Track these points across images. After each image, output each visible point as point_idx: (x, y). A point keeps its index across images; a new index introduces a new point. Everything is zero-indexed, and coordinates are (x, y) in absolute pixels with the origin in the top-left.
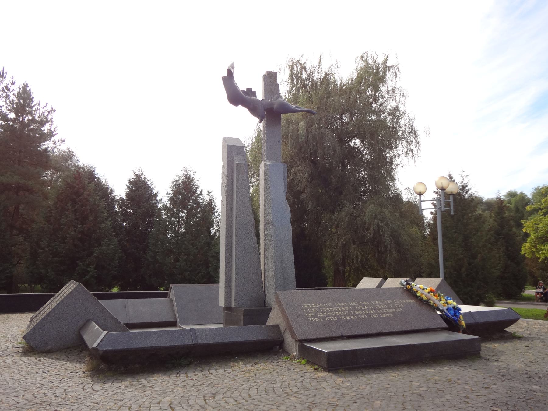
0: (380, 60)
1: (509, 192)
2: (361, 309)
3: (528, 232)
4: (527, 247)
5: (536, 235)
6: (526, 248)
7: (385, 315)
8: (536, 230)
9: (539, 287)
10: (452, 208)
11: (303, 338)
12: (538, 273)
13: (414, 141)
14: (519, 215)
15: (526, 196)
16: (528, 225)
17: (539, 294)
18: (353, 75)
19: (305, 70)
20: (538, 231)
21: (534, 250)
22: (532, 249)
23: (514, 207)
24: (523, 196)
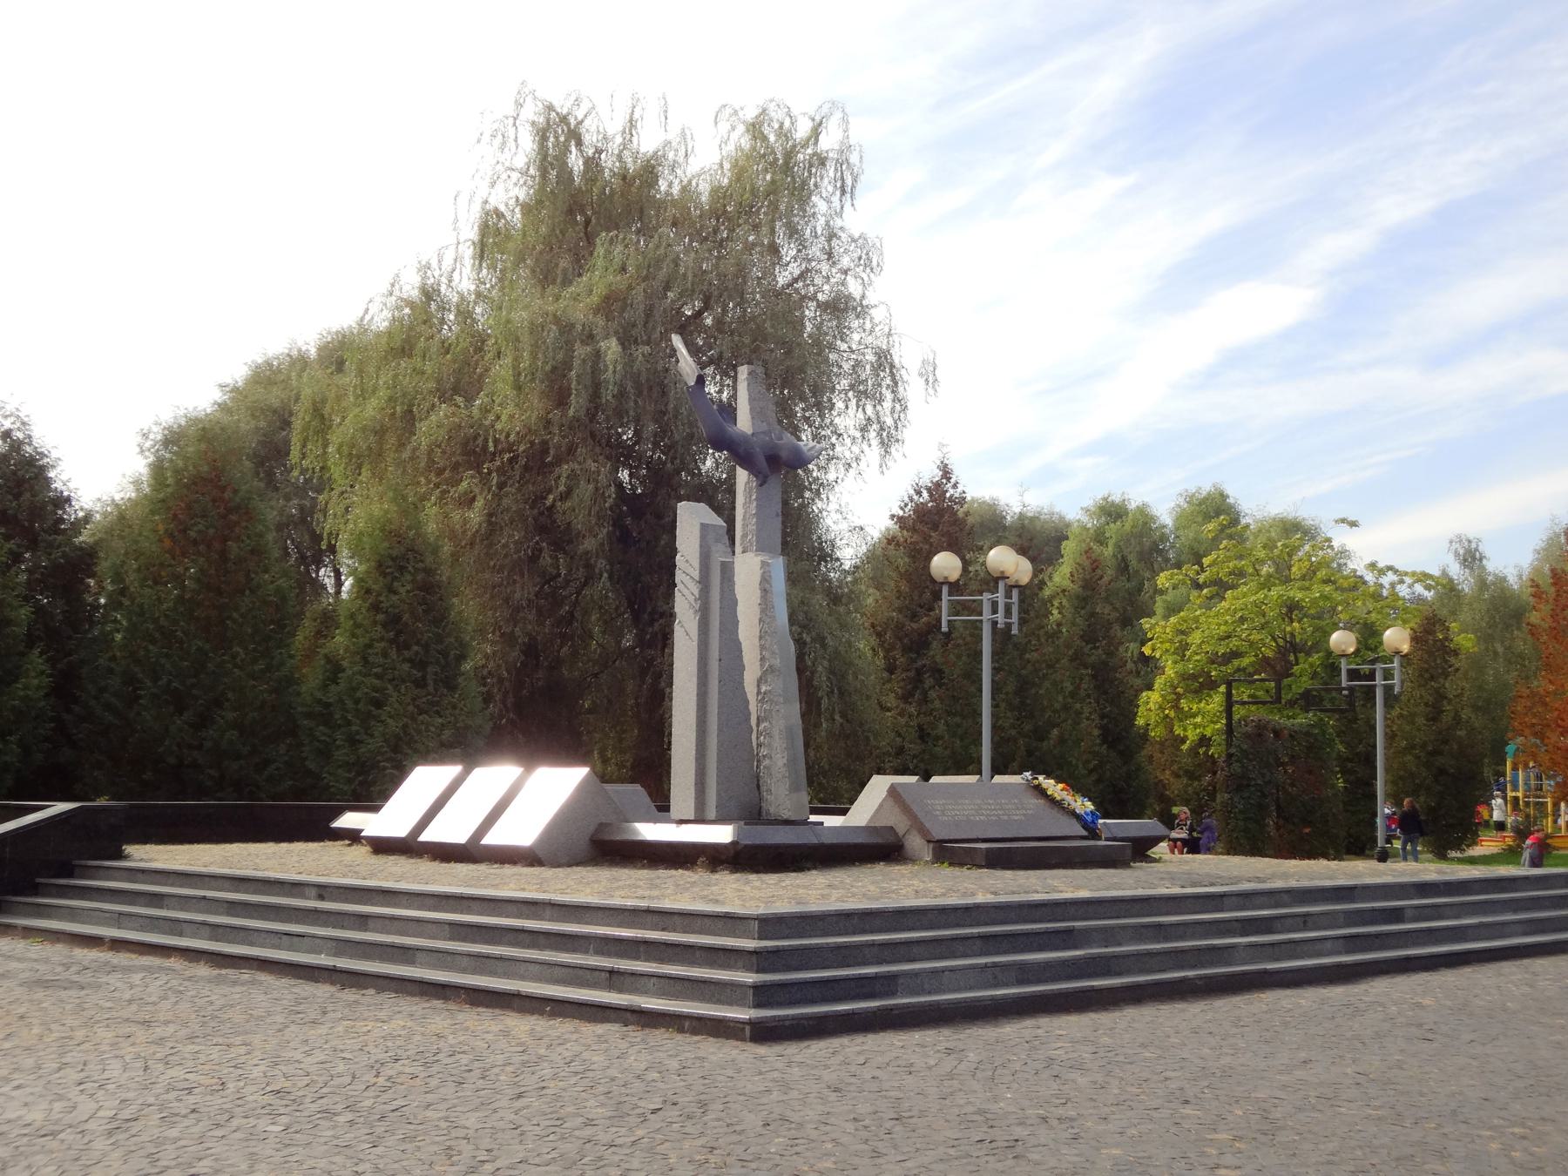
0: (802, 130)
1: (1105, 499)
2: (988, 809)
3: (1158, 656)
4: (1151, 705)
5: (1180, 667)
6: (1150, 704)
7: (1016, 818)
8: (1182, 650)
9: (1178, 825)
10: (1015, 619)
11: (941, 838)
12: (1176, 786)
13: (888, 395)
14: (1128, 585)
15: (1153, 519)
16: (1158, 630)
17: (1179, 843)
18: (742, 196)
19: (579, 143)
20: (1188, 653)
21: (1172, 714)
22: (1167, 712)
23: (1114, 556)
24: (1144, 518)
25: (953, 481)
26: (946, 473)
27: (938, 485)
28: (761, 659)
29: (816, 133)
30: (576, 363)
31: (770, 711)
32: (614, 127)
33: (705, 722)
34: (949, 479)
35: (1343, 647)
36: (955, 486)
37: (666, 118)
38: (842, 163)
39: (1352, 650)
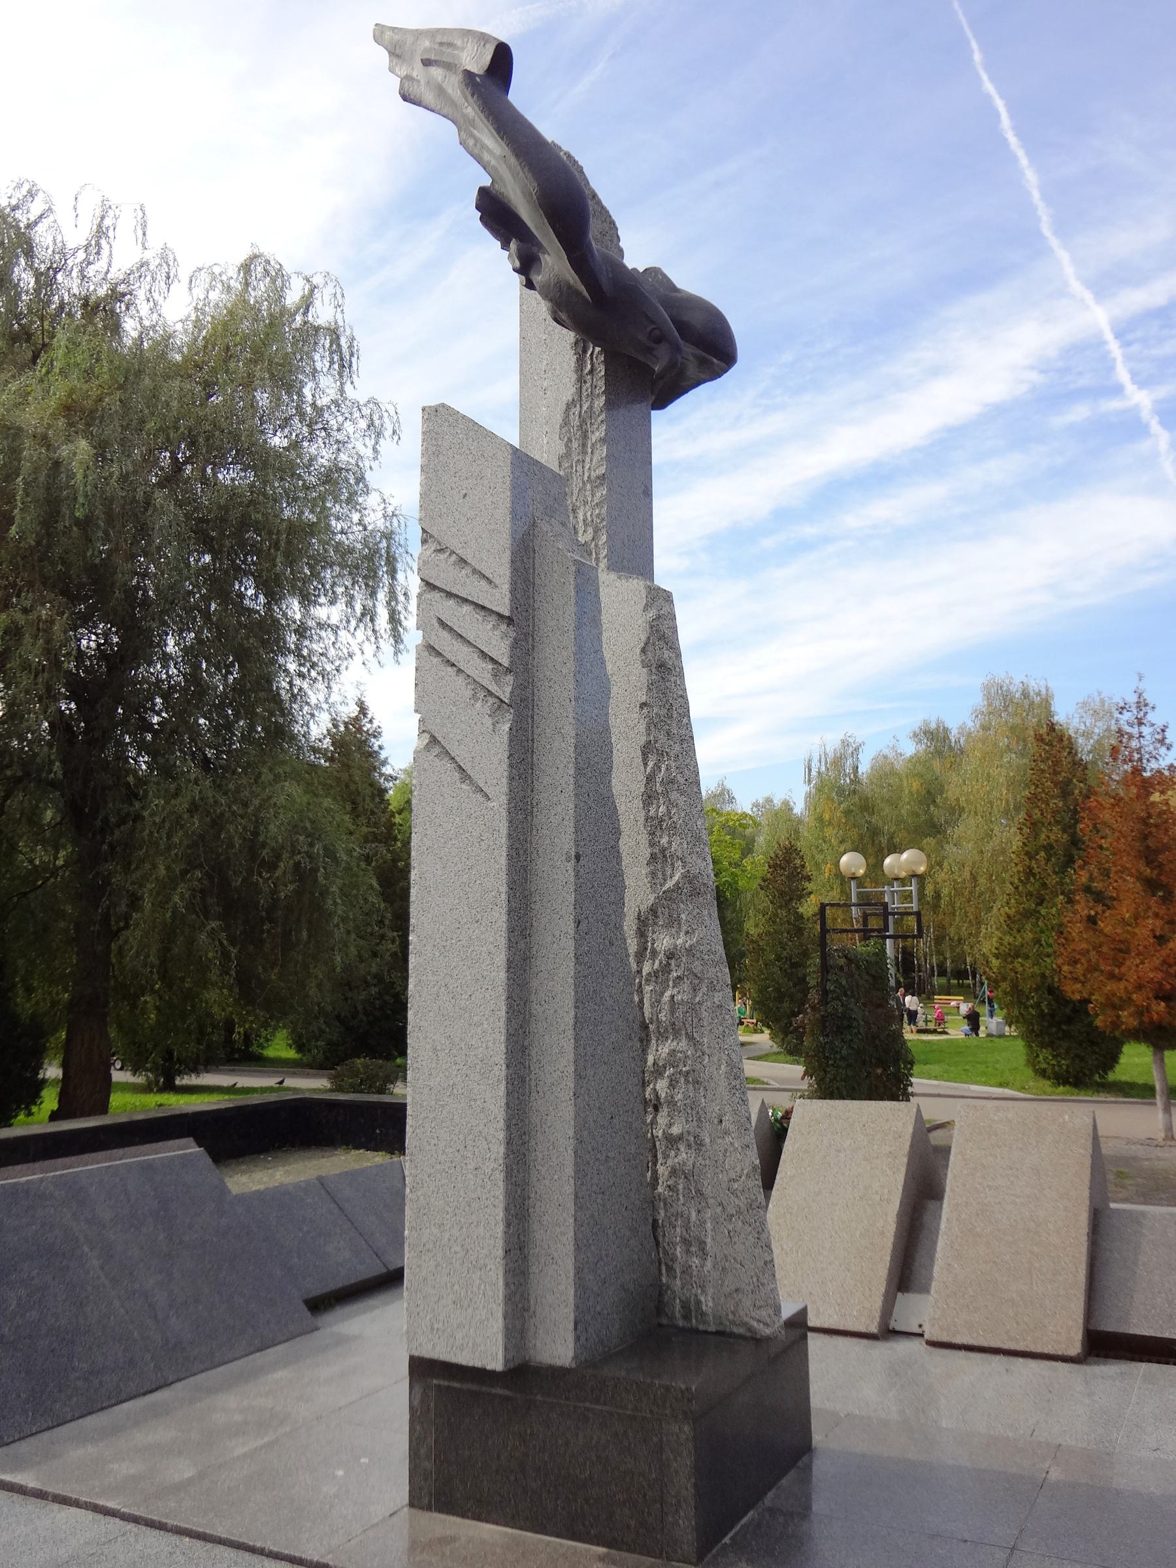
25: (369, 716)
26: (363, 709)
27: (357, 719)
28: (653, 857)
29: (307, 303)
30: (26, 466)
31: (693, 1008)
32: (76, 236)
33: (524, 1049)
34: (365, 715)
35: (853, 870)
36: (371, 722)
37: (144, 234)
38: (334, 333)
39: (862, 872)
